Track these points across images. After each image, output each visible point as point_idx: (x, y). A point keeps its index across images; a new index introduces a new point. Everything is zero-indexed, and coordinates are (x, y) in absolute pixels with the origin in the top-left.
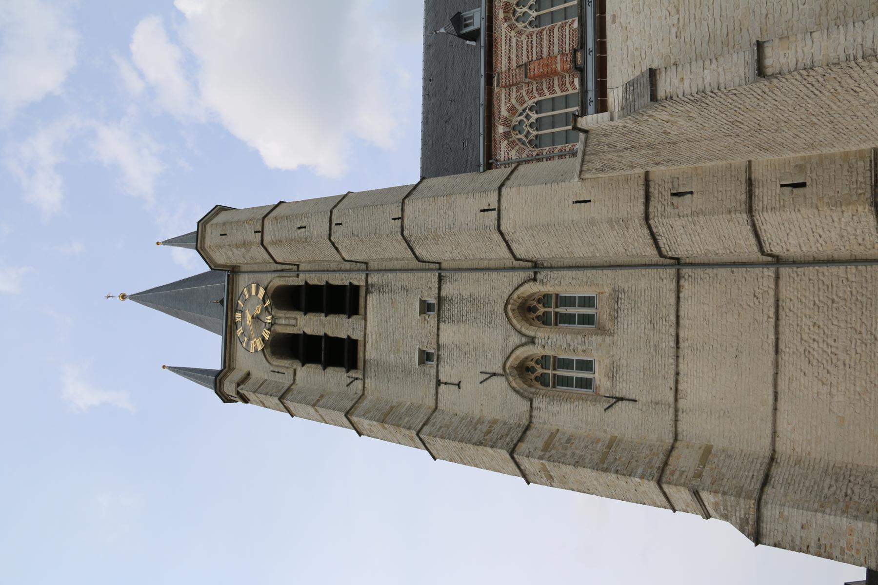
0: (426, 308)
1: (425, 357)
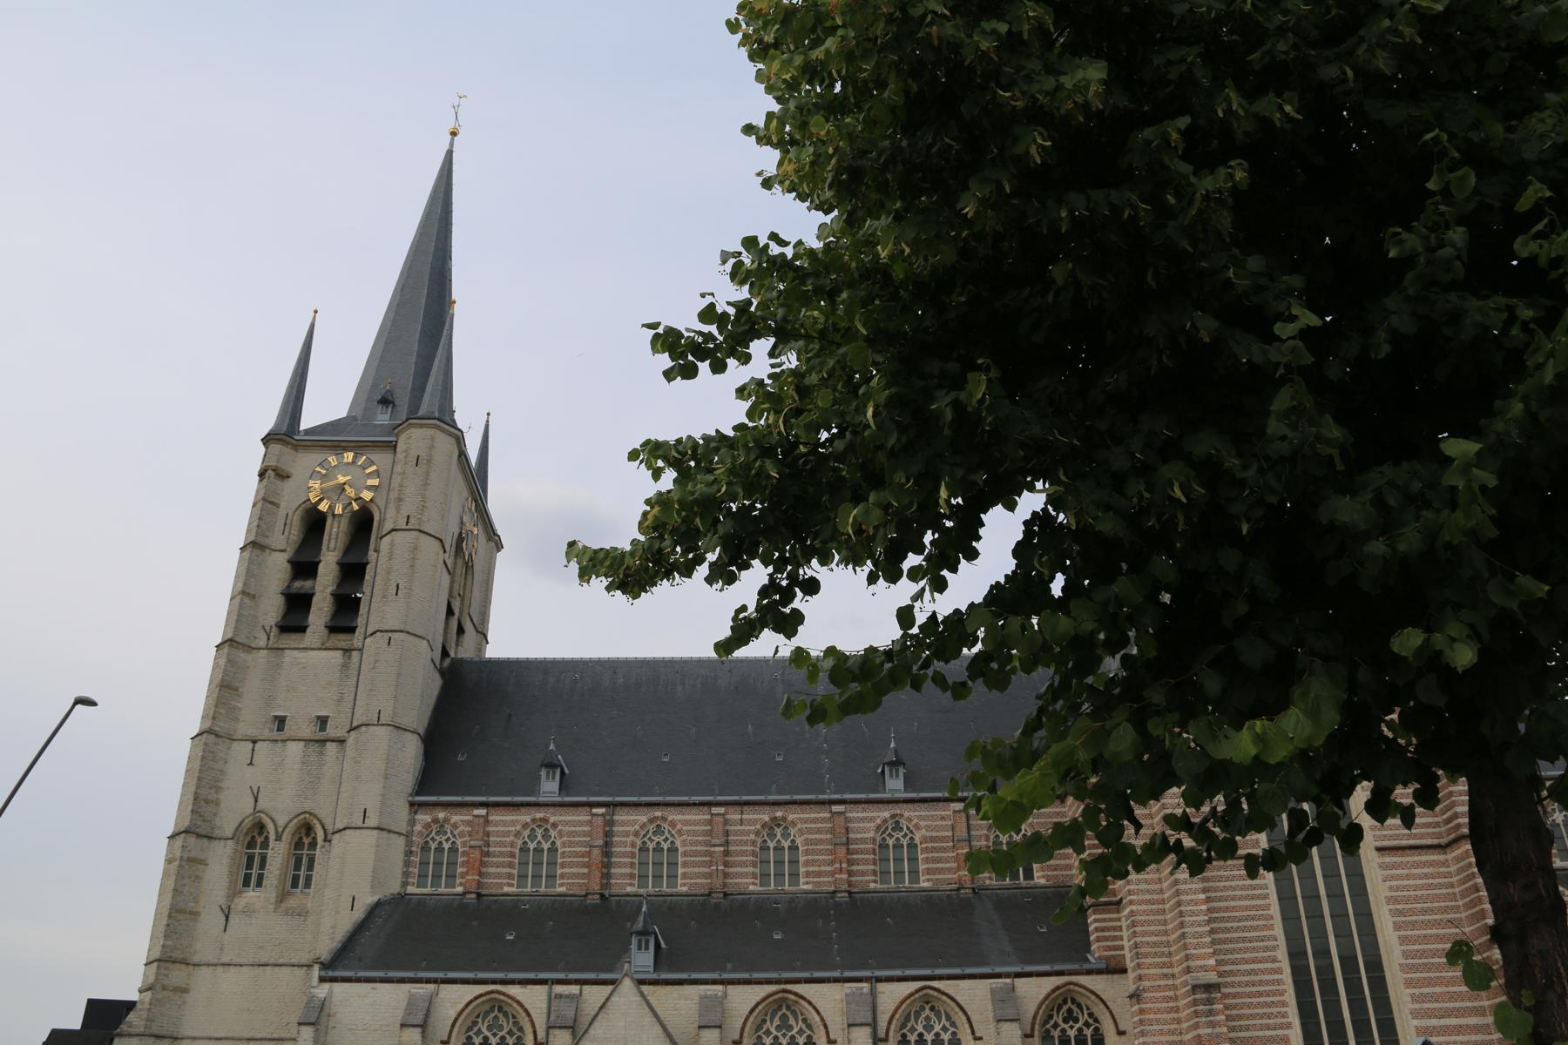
0: (323, 721)
1: (281, 722)
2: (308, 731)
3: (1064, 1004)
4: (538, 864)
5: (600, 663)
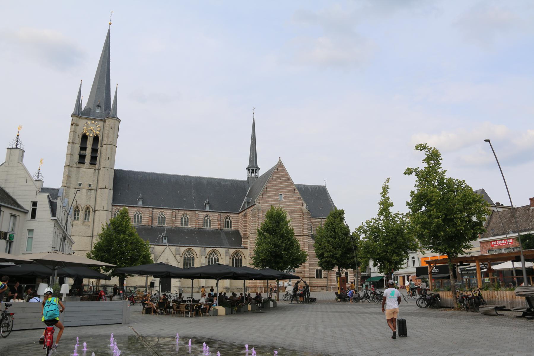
0: (90, 185)
1: (80, 184)
2: (87, 187)
3: (236, 253)
4: (138, 219)
5: (146, 173)
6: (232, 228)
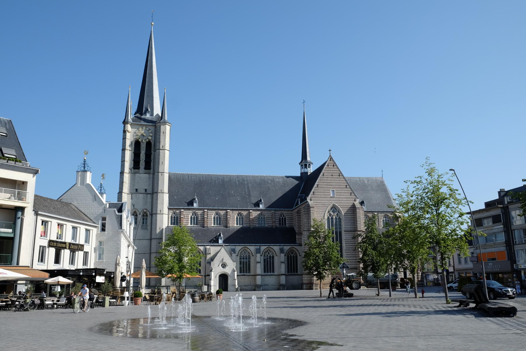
6: (287, 225)
